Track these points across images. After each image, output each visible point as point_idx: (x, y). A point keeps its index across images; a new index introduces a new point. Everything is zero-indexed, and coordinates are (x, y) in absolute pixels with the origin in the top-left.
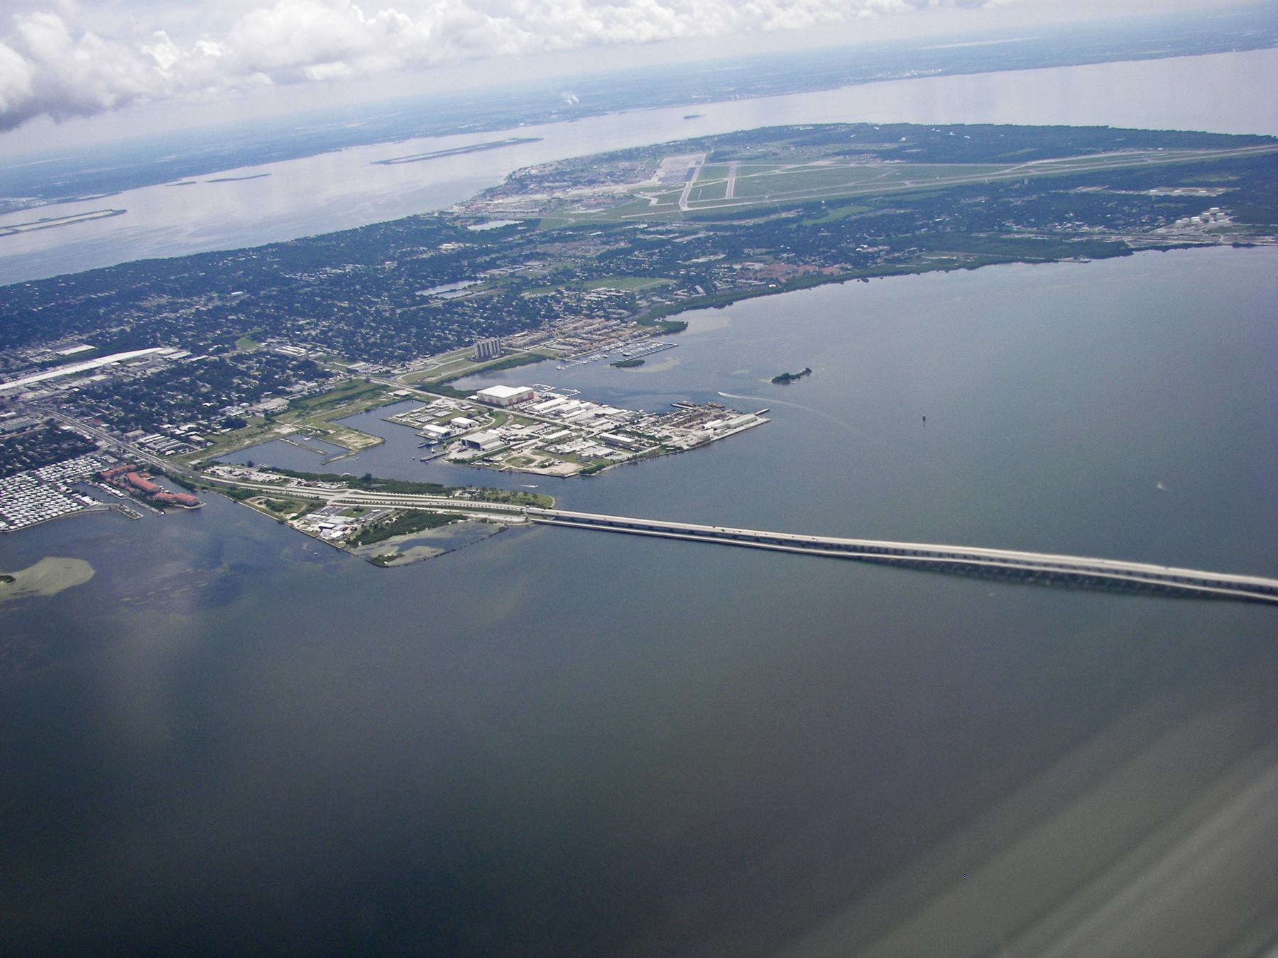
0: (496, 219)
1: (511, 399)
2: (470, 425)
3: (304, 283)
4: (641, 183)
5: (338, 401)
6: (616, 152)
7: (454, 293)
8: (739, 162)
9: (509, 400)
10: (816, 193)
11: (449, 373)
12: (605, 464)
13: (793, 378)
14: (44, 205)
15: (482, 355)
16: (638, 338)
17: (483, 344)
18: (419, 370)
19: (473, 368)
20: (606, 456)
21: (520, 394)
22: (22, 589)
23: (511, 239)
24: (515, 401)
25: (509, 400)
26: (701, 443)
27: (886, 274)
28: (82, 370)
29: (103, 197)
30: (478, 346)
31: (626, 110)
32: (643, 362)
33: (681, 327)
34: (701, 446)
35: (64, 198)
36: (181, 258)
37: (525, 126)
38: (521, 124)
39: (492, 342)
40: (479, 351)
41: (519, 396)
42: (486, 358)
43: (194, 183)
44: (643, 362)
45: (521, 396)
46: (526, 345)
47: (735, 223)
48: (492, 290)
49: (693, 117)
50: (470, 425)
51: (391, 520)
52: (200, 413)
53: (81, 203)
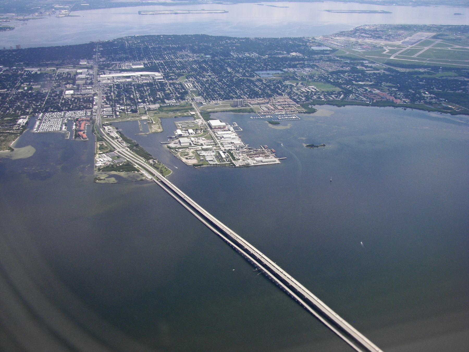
0: (326, 46)
1: (216, 127)
2: (191, 133)
3: (245, 56)
4: (394, 42)
5: (177, 110)
6: (405, 25)
7: (268, 75)
8: (442, 40)
9: (215, 127)
10: (450, 62)
11: (218, 109)
12: (204, 164)
13: (315, 147)
14: (211, 4)
15: (235, 104)
16: (293, 112)
17: (236, 101)
18: (212, 105)
19: (228, 109)
20: (209, 161)
21: (220, 125)
22: (10, 155)
23: (316, 56)
24: (217, 127)
25: (215, 127)
26: (245, 165)
27: (415, 108)
28: (128, 75)
29: (231, 4)
30: (234, 101)
31: (438, 6)
32: (279, 124)
33: (314, 111)
34: (244, 167)
35: (220, 2)
36: (155, 36)
37: (395, 5)
38: (394, 4)
39: (240, 101)
40: (234, 103)
41: (219, 126)
42: (236, 106)
43: (263, 5)
44: (279, 124)
45: (220, 126)
46: (256, 104)
47: (394, 68)
48: (279, 77)
49: (458, 14)
50: (191, 133)
51: (119, 164)
52: (23, 109)
53: (223, 5)
